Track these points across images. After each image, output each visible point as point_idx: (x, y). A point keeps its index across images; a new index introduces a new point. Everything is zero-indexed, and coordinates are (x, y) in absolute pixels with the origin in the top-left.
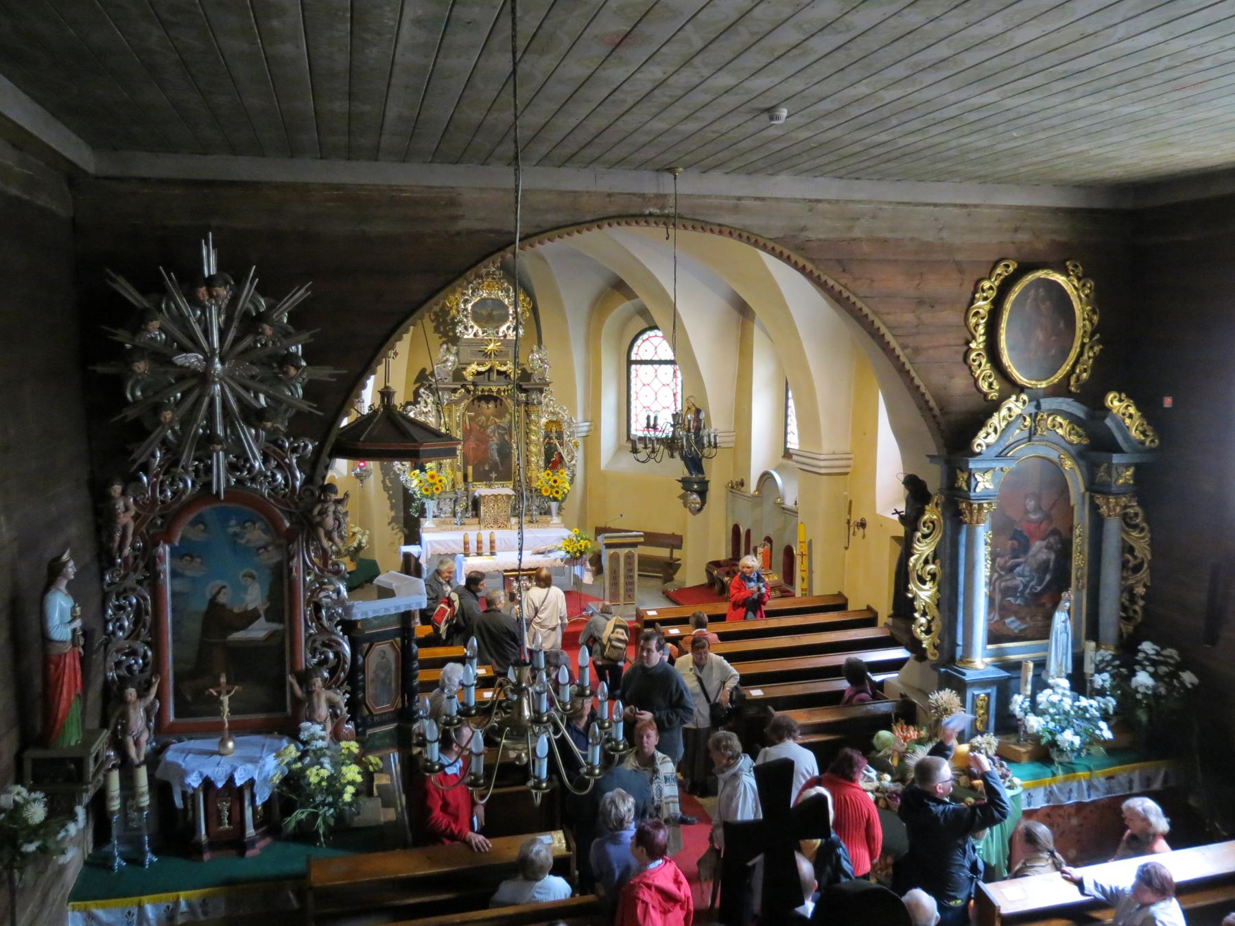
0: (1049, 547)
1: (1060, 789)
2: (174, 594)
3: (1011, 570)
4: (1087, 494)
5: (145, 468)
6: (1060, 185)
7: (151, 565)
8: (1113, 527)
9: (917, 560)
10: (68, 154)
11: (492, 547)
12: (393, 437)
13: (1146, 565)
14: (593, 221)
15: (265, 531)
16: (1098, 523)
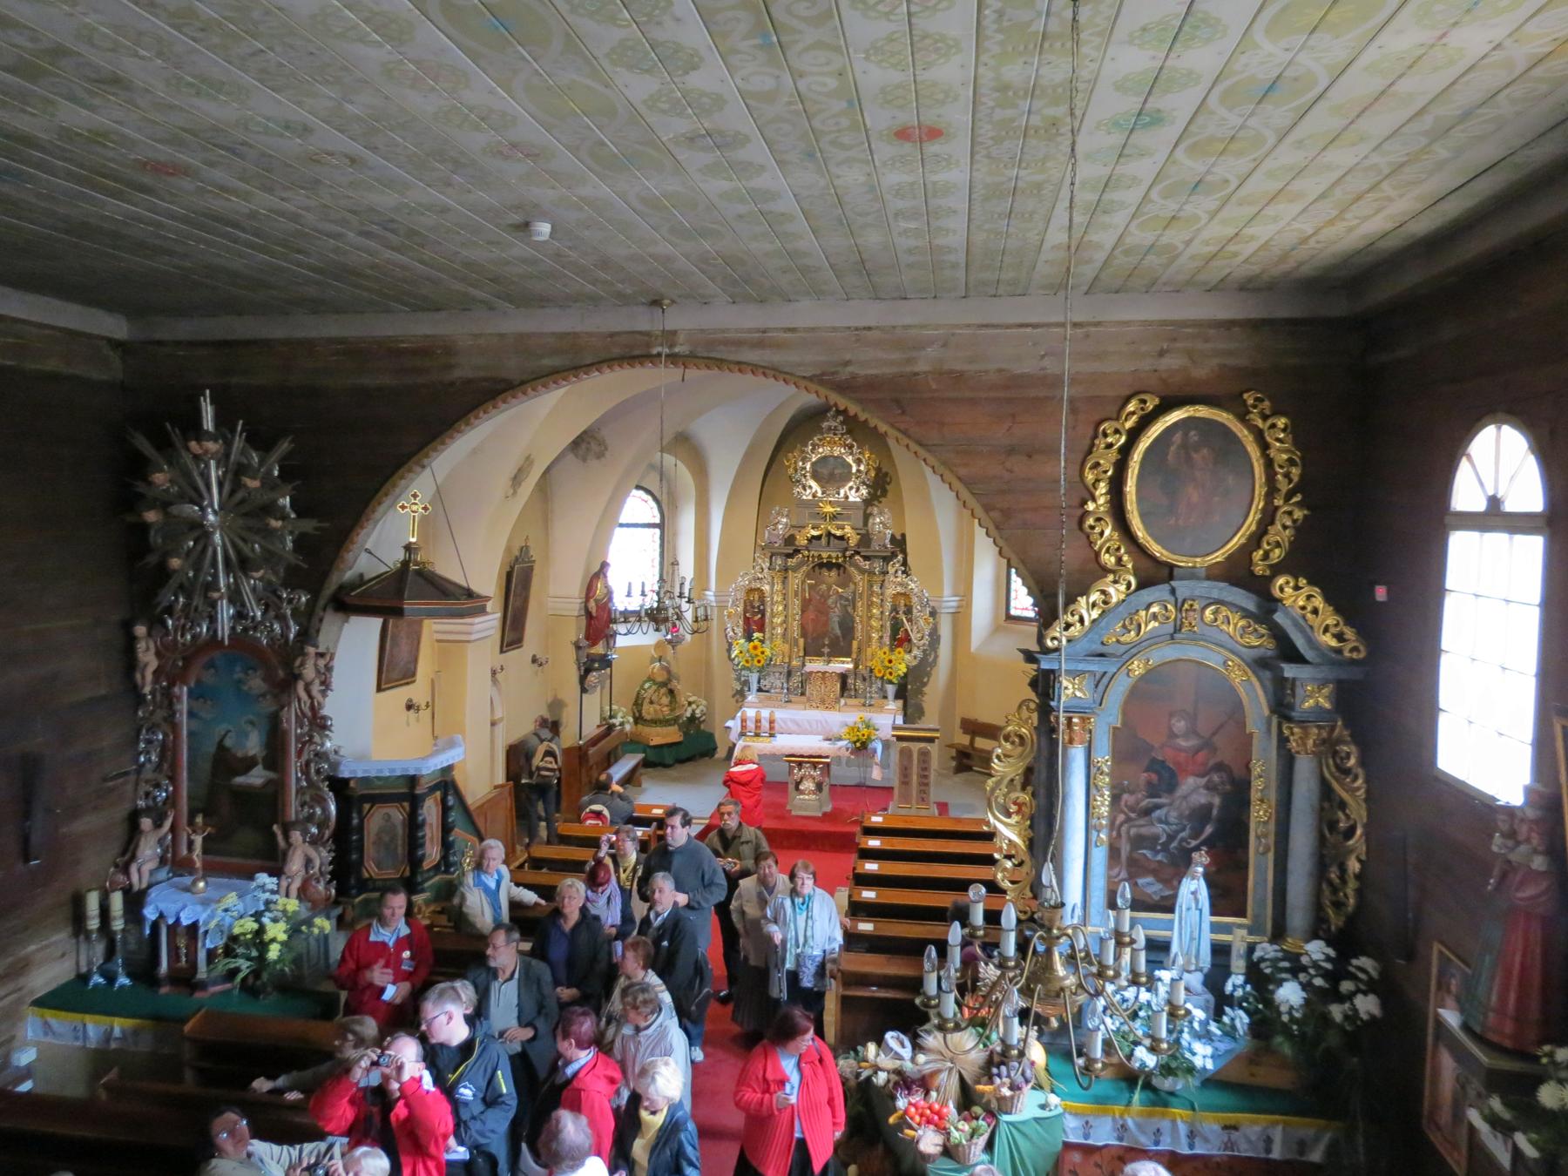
0: (1210, 787)
1: (1138, 1125)
2: (191, 734)
3: (1147, 812)
4: (1275, 720)
5: (169, 610)
6: (1218, 288)
7: (169, 700)
8: (1305, 769)
9: (998, 784)
10: (61, 323)
11: (771, 728)
12: (404, 595)
13: (1359, 832)
14: (592, 365)
15: (264, 680)
16: (1287, 762)
